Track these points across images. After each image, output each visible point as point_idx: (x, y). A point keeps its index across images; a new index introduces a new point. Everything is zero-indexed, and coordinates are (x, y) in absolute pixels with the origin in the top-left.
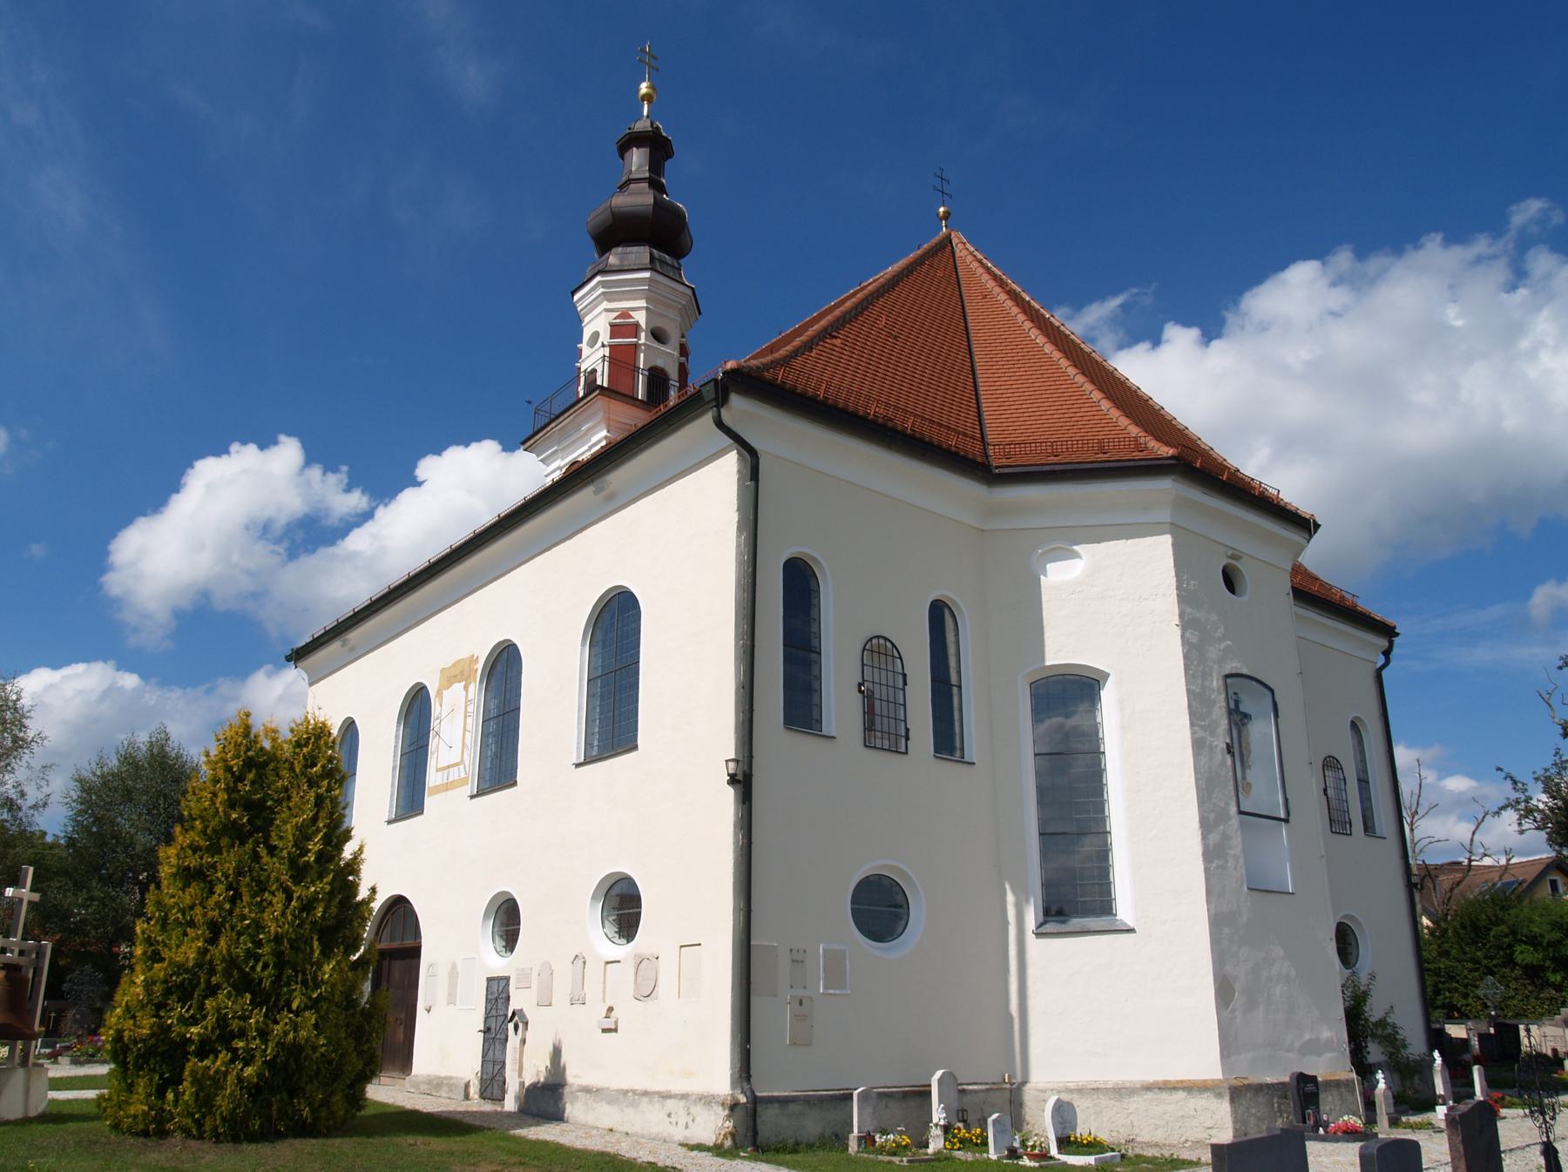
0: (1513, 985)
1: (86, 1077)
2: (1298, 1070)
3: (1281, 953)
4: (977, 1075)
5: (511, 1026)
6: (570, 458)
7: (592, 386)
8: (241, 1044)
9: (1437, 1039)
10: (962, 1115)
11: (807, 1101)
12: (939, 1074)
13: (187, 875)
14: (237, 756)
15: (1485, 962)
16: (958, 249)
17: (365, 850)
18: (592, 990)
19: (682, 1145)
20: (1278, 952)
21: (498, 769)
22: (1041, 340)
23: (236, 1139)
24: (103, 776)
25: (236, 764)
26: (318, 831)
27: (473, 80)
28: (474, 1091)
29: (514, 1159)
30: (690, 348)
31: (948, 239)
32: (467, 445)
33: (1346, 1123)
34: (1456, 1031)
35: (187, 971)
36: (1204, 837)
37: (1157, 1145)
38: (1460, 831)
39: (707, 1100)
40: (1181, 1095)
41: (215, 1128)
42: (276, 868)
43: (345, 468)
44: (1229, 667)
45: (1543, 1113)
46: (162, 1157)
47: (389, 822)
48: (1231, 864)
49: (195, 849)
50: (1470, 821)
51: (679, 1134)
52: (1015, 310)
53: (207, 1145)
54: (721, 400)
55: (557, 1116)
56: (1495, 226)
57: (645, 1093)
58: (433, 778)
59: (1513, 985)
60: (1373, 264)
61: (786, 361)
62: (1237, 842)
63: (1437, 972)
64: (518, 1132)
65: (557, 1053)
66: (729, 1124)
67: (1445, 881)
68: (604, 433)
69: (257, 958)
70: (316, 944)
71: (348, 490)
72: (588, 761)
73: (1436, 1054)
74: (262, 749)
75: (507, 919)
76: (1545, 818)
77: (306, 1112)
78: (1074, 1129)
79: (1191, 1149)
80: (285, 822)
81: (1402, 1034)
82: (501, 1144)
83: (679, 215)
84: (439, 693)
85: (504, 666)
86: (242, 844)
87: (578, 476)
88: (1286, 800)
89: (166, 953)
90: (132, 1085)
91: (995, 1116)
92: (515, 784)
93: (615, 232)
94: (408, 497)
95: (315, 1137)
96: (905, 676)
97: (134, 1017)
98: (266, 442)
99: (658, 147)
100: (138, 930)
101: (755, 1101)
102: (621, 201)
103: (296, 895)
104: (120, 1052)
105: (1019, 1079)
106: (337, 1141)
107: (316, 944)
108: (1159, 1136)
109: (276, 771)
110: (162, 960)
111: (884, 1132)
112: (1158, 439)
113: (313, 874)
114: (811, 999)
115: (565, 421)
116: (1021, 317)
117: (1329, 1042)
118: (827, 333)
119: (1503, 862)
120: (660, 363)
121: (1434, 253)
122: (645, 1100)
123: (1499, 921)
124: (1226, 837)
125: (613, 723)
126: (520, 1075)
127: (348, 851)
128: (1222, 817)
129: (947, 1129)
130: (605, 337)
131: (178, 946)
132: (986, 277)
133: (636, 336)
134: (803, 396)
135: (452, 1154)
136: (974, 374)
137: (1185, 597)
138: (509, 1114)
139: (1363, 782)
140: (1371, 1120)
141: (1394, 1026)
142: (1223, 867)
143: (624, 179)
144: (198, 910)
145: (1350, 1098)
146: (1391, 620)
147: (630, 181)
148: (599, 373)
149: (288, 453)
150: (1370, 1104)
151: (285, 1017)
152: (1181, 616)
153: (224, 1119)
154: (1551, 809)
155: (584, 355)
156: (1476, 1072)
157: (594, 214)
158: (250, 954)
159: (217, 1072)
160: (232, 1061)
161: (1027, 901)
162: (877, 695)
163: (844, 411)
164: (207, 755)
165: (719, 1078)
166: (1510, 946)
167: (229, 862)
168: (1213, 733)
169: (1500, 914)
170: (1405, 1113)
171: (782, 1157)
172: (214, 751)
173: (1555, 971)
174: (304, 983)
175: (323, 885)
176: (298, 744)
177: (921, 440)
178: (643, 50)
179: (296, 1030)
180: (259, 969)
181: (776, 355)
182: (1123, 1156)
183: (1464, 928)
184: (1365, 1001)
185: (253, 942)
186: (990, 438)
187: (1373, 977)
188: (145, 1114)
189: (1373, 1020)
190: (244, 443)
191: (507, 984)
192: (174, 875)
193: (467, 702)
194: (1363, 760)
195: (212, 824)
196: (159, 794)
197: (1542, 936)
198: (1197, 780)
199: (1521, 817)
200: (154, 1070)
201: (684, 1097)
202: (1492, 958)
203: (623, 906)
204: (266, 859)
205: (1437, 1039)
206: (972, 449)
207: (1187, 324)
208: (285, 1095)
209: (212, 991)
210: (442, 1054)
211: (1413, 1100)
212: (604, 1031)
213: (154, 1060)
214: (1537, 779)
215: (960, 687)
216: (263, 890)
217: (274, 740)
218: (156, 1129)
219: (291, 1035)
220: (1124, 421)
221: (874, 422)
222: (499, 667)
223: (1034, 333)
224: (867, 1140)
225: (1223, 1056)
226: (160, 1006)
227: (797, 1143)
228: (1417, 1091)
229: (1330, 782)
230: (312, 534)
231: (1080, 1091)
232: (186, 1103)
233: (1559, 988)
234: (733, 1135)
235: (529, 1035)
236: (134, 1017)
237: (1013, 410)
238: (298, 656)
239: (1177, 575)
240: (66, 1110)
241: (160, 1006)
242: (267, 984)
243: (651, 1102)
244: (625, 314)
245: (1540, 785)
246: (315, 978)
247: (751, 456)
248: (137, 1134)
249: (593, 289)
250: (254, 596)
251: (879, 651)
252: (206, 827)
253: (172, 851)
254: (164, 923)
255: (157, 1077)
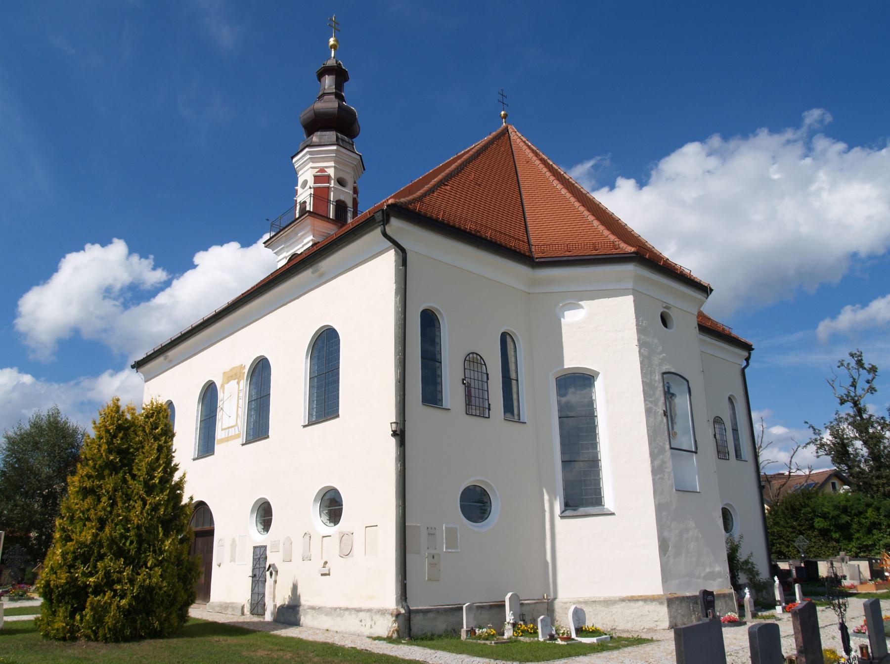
0: (813, 540)
1: (21, 608)
2: (703, 589)
3: (694, 525)
4: (529, 596)
5: (268, 573)
6: (291, 252)
7: (303, 211)
8: (119, 587)
9: (774, 570)
10: (522, 617)
11: (438, 611)
12: (509, 595)
13: (85, 492)
14: (112, 424)
15: (798, 528)
16: (512, 135)
17: (187, 476)
18: (315, 551)
19: (369, 637)
20: (692, 524)
21: (258, 427)
22: (559, 186)
23: (117, 641)
24: (21, 435)
25: (112, 429)
26: (160, 465)
27: (226, 36)
28: (247, 610)
29: (276, 648)
30: (359, 189)
31: (506, 130)
32: (222, 245)
33: (729, 617)
34: (783, 566)
35: (86, 546)
36: (652, 462)
37: (628, 631)
38: (783, 457)
39: (382, 612)
40: (641, 603)
41: (105, 635)
42: (137, 487)
43: (152, 257)
44: (665, 368)
45: (840, 608)
46: (76, 652)
47: (194, 459)
48: (666, 476)
49: (89, 477)
50: (794, 452)
51: (367, 631)
52: (545, 170)
53: (100, 644)
54: (386, 221)
55: (296, 623)
56: (797, 124)
57: (347, 609)
58: (219, 434)
59: (813, 540)
60: (733, 144)
61: (420, 199)
62: (669, 465)
63: (773, 534)
64: (275, 632)
65: (295, 588)
66: (395, 625)
67: (776, 484)
68: (311, 237)
69: (127, 538)
70: (160, 529)
71: (154, 268)
72: (310, 424)
73: (776, 578)
74: (126, 419)
75: (264, 514)
76: (831, 449)
77: (157, 624)
78: (584, 623)
79: (646, 633)
80: (141, 461)
81: (757, 568)
82: (268, 639)
83: (352, 114)
84: (222, 386)
85: (260, 370)
86: (116, 474)
87: (297, 265)
88: (695, 441)
89: (74, 536)
90: (55, 611)
91: (542, 617)
92: (268, 437)
93: (316, 124)
94: (190, 275)
95: (162, 638)
96: (487, 375)
97: (56, 573)
98: (105, 242)
99: (340, 75)
100: (57, 523)
101: (410, 612)
102: (320, 106)
103: (148, 502)
104: (47, 592)
105: (552, 597)
106: (175, 640)
107: (160, 529)
108: (629, 626)
109: (135, 431)
110: (71, 540)
111: (480, 628)
112: (626, 243)
113: (158, 490)
114: (438, 555)
115: (289, 231)
116: (548, 174)
117: (719, 572)
118: (442, 183)
119: (807, 473)
120: (342, 198)
121: (764, 139)
122: (347, 613)
123: (806, 505)
124: (663, 462)
125: (324, 402)
126: (274, 601)
127: (176, 477)
128: (662, 451)
129: (514, 625)
130: (311, 183)
131: (81, 532)
132: (528, 151)
133: (329, 182)
134: (431, 219)
135: (241, 646)
136: (522, 206)
137: (641, 330)
138: (268, 623)
139: (735, 430)
140: (742, 614)
141: (752, 564)
142: (662, 479)
143: (321, 93)
144: (92, 511)
145: (731, 603)
146: (749, 341)
147: (324, 94)
148: (308, 204)
149: (119, 248)
150: (741, 607)
151: (144, 571)
152: (639, 340)
153: (110, 629)
154: (834, 444)
155: (299, 193)
156: (797, 588)
157: (303, 113)
158: (122, 536)
159: (105, 603)
160: (114, 596)
161: (556, 499)
162: (472, 385)
163: (453, 227)
164: (95, 423)
165: (389, 599)
166: (812, 519)
167: (109, 483)
168: (656, 405)
169: (807, 501)
170: (760, 611)
171: (425, 642)
172: (99, 420)
173: (836, 532)
174: (154, 551)
175: (164, 496)
176: (147, 417)
177: (496, 243)
178: (331, 20)
179: (150, 578)
180: (128, 544)
181: (415, 196)
182: (611, 638)
183: (787, 509)
184: (737, 551)
185: (124, 529)
186: (532, 242)
187: (741, 537)
188: (64, 628)
189: (741, 560)
190: (93, 243)
191: (265, 550)
192: (77, 492)
193: (239, 391)
194: (735, 419)
195: (99, 462)
196: (54, 445)
197: (829, 513)
198: (648, 431)
199: (818, 448)
200: (68, 603)
201: (369, 610)
202: (802, 526)
203: (332, 505)
204: (131, 482)
205: (774, 570)
206: (524, 248)
207: (628, 177)
208: (144, 615)
209: (101, 557)
210: (228, 590)
211: (764, 603)
212: (322, 575)
213: (68, 597)
214: (826, 428)
215: (517, 380)
216: (130, 500)
217: (133, 414)
218: (70, 636)
219: (148, 581)
220: (606, 232)
221: (470, 233)
222: (257, 370)
223: (556, 183)
224: (471, 632)
225: (663, 582)
226: (71, 566)
227: (433, 635)
228: (764, 599)
229: (717, 431)
230: (136, 295)
231: (586, 602)
232: (88, 621)
233: (837, 541)
234: (398, 631)
235: (278, 578)
236: (56, 573)
237: (545, 226)
238: (138, 365)
239: (637, 318)
240: (14, 627)
241: (71, 566)
242: (133, 552)
243: (350, 614)
244: (322, 170)
245: (828, 431)
246: (160, 549)
247: (402, 253)
248: (59, 639)
249: (304, 156)
250: (105, 330)
251: (474, 361)
252: (95, 464)
253: (76, 478)
254: (72, 519)
255: (70, 607)
